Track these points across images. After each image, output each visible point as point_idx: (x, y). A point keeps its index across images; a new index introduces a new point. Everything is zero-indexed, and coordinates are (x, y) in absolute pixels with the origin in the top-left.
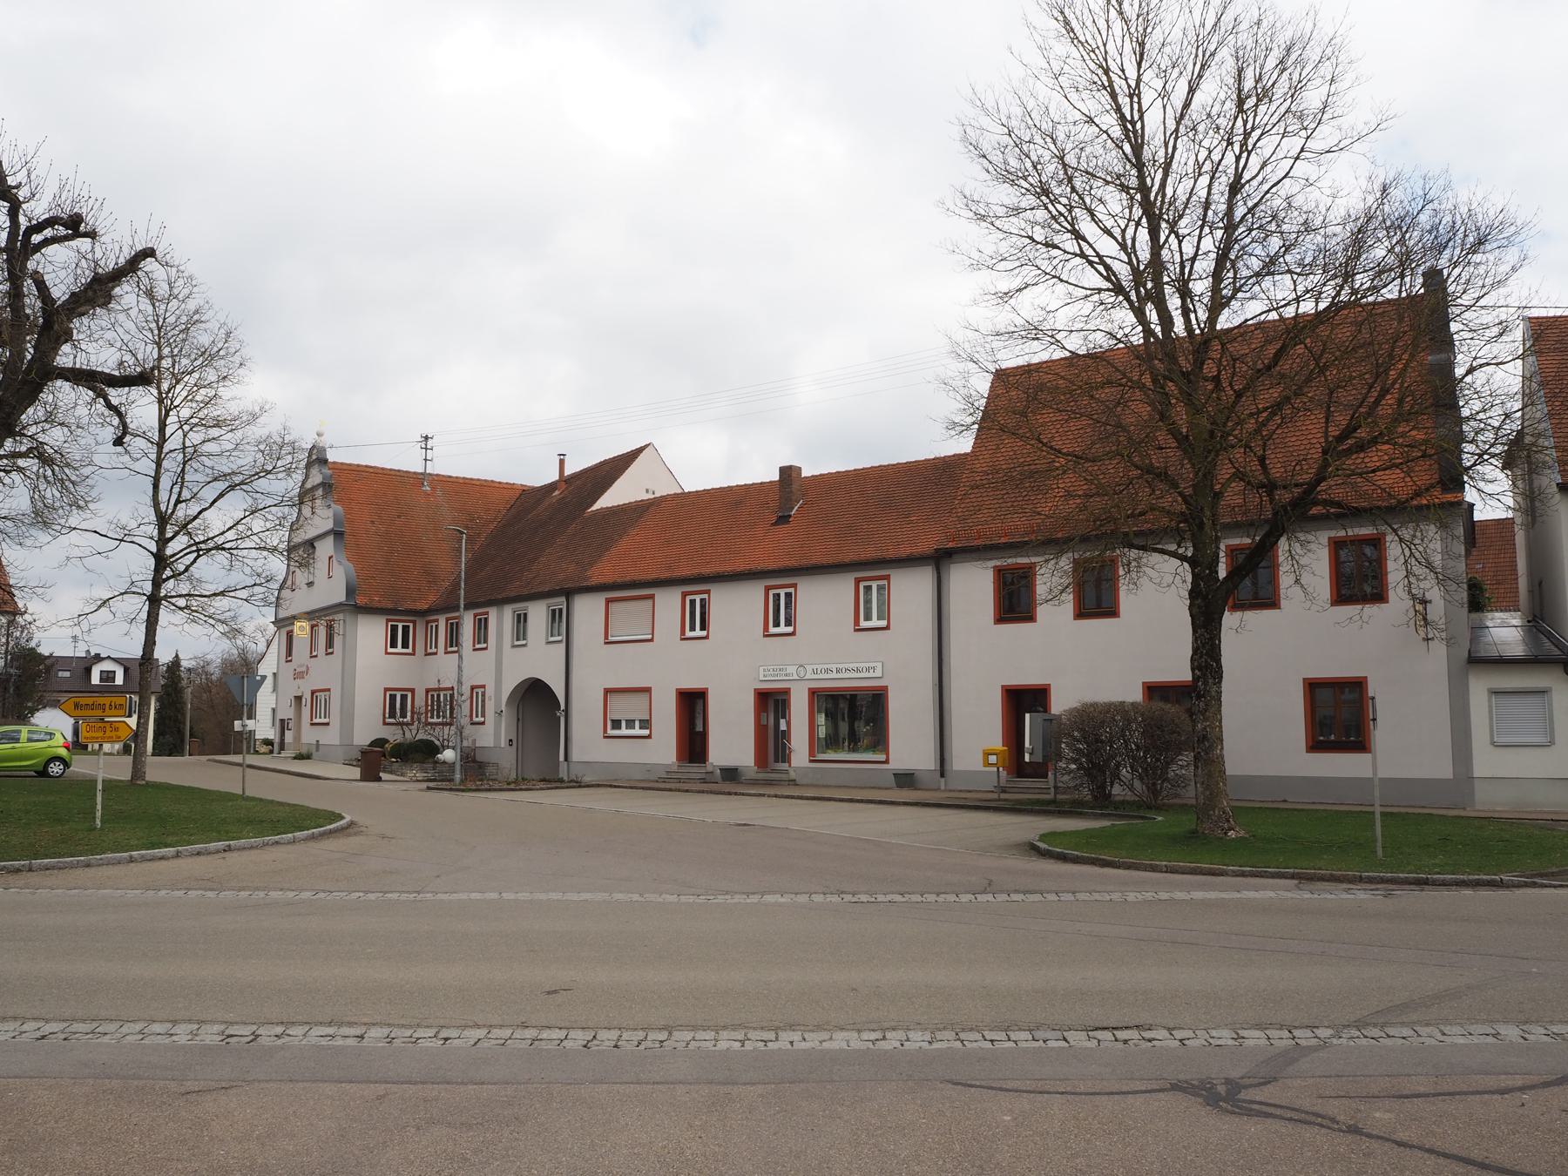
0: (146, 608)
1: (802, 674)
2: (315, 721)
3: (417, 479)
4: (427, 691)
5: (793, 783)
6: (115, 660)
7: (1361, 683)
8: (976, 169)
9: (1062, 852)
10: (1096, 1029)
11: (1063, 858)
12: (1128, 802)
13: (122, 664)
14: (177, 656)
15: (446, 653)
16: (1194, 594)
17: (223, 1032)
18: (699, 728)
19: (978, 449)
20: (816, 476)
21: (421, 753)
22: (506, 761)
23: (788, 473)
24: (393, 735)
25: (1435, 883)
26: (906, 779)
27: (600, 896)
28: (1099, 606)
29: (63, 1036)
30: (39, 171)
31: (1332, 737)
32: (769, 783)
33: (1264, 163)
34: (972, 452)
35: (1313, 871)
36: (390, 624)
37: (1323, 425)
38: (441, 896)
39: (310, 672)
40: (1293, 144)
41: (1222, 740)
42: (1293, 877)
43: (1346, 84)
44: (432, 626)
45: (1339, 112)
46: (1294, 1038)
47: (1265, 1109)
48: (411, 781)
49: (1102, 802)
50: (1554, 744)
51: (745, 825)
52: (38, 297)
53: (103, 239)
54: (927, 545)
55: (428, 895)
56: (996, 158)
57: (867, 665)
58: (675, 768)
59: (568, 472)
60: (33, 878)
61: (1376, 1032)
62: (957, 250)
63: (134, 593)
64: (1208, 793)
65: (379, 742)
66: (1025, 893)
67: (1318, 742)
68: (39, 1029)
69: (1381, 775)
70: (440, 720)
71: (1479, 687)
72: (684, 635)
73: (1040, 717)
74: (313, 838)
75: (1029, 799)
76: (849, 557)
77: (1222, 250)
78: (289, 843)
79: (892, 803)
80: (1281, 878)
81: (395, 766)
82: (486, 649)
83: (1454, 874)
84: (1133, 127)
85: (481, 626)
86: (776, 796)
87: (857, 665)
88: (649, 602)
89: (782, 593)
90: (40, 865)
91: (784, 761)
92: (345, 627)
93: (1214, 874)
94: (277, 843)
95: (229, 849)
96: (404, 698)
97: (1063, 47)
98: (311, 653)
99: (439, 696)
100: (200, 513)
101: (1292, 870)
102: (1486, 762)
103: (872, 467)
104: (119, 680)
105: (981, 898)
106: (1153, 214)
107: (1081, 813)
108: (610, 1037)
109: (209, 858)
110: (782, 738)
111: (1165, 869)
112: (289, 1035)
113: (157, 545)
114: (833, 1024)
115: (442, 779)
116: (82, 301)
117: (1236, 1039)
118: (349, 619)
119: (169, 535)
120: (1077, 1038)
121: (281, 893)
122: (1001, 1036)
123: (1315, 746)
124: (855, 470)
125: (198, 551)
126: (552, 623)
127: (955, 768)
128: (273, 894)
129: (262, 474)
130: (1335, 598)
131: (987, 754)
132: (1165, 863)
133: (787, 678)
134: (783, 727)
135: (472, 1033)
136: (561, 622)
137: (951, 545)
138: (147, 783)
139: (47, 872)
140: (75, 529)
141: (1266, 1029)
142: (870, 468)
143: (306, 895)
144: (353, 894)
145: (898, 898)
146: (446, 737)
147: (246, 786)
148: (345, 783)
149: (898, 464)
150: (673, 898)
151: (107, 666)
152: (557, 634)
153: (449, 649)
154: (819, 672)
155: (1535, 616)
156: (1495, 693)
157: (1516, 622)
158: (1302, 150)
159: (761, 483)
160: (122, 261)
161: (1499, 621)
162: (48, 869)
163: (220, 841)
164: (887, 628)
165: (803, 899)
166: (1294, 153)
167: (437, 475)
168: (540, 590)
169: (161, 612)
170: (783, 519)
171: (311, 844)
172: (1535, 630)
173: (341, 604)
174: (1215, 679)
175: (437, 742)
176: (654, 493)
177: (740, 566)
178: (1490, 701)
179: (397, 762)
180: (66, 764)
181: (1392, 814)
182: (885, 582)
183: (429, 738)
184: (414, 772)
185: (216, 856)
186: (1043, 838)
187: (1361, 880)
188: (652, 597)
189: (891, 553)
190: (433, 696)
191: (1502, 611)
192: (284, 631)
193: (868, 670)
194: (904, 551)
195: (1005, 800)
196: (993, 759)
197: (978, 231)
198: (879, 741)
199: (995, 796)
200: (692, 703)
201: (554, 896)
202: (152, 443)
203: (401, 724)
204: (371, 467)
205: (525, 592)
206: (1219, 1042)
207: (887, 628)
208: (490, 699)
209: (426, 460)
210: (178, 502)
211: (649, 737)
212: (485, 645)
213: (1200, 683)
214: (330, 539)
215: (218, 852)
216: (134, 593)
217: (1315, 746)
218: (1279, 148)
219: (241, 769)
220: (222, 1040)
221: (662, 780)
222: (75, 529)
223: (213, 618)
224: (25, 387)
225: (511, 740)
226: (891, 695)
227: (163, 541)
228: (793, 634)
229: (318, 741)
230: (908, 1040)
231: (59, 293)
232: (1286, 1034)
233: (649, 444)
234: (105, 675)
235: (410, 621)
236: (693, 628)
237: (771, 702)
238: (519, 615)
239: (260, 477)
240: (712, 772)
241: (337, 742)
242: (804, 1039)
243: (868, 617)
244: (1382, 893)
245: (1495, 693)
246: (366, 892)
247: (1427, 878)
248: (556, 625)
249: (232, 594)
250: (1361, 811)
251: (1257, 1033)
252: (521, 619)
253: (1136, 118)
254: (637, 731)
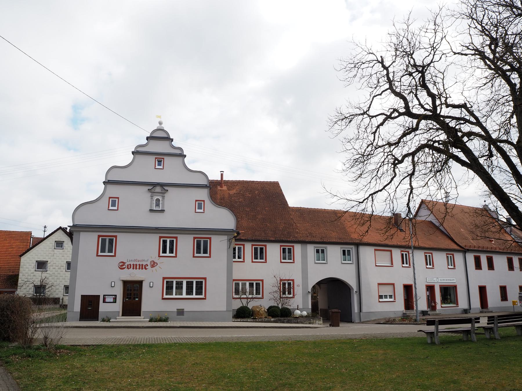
36: (282, 247)
67: (502, 300)
77: (516, 178)
87: (450, 279)
193: (453, 280)
200: (408, 289)
226: (163, 277)
237: (430, 289)
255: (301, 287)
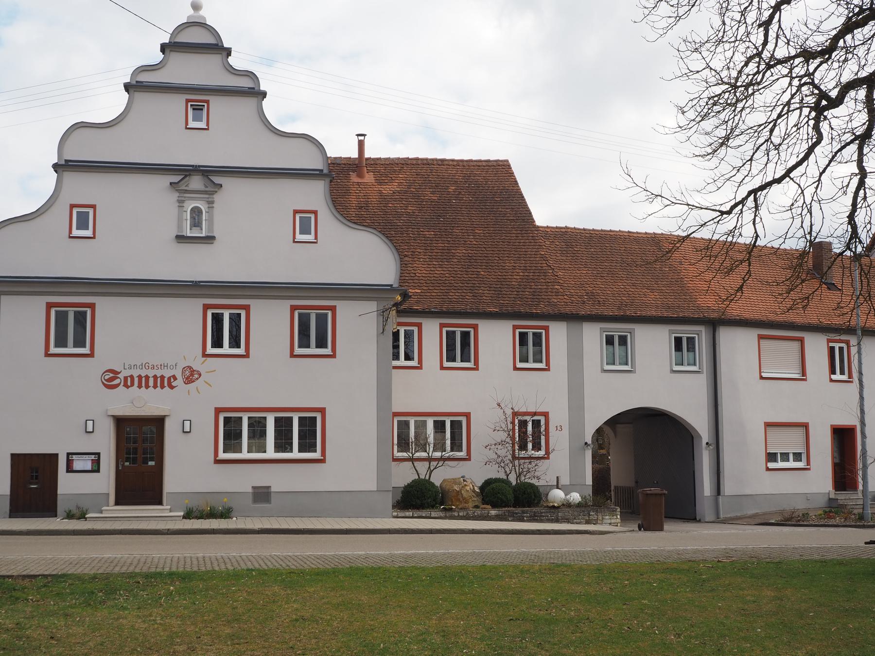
208: (560, 428)
241: (373, 487)
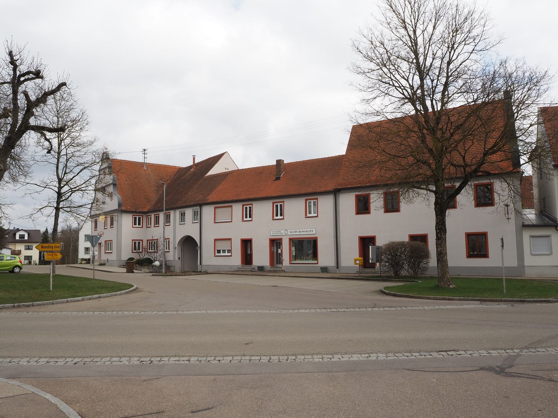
0: (54, 211)
1: (286, 233)
2: (106, 252)
3: (142, 165)
4: (148, 241)
5: (284, 271)
6: (25, 231)
7: (485, 234)
8: (360, 57)
9: (395, 294)
10: (440, 352)
11: (395, 295)
12: (407, 276)
13: (27, 232)
14: (47, 229)
15: (154, 227)
16: (436, 204)
17: (139, 360)
18: (249, 252)
19: (348, 153)
20: (289, 163)
21: (146, 263)
22: (178, 266)
23: (279, 162)
24: (136, 256)
25: (527, 302)
26: (324, 269)
27: (242, 311)
28: (393, 208)
29: (83, 363)
30: (25, 54)
31: (475, 253)
32: (275, 271)
33: (459, 54)
34: (345, 155)
35: (485, 298)
36: (134, 216)
37: (483, 147)
38: (185, 312)
39: (104, 234)
40: (470, 48)
41: (447, 254)
42: (478, 300)
43: (489, 27)
44: (149, 217)
45: (487, 37)
46: (507, 353)
47: (519, 375)
48: (144, 273)
49: (397, 277)
50: (552, 254)
51: (275, 286)
52: (26, 100)
53: (45, 79)
54: (331, 187)
55: (181, 312)
56: (364, 52)
57: (310, 230)
58: (241, 267)
59: (196, 162)
60: (36, 308)
61: (533, 350)
62: (352, 84)
63: (50, 206)
64: (442, 272)
65: (131, 259)
66: (389, 307)
68: (72, 360)
69: (505, 265)
70: (153, 251)
71: (526, 235)
72: (274, 218)
73: (374, 247)
74: (126, 293)
75: (373, 276)
76: (303, 192)
78: (119, 295)
79: (322, 278)
80: (474, 301)
81: (138, 267)
82: (170, 225)
83: (533, 298)
84: (414, 41)
85: (168, 218)
86: (280, 276)
87: (306, 230)
88: (231, 208)
89: (279, 204)
90: (36, 304)
91: (280, 264)
92: (118, 218)
93: (450, 300)
94: (116, 295)
95: (100, 297)
96: (139, 243)
97: (391, 14)
98: (104, 227)
99: (152, 242)
100: (73, 177)
101: (477, 298)
102: (529, 261)
103: (309, 160)
104: (26, 238)
105: (375, 309)
106: (422, 72)
107: (391, 280)
108: (276, 358)
109: (94, 300)
110: (279, 256)
111: (433, 299)
112: (163, 361)
113: (58, 189)
114: (350, 352)
115: (157, 271)
116: (40, 101)
117: (488, 354)
118: (119, 215)
119: (62, 185)
120: (435, 354)
121: (128, 312)
122: (409, 354)
123: (469, 256)
124: (303, 161)
125: (72, 191)
126: (194, 216)
127: (342, 265)
128: (125, 313)
129: (95, 164)
130: (476, 204)
131: (356, 260)
132: (433, 296)
133: (281, 234)
134: (279, 251)
135: (227, 358)
136: (198, 217)
137: (340, 187)
138: (56, 274)
139: (39, 306)
140: (28, 183)
141: (496, 350)
142: (308, 160)
143: (137, 313)
144: (154, 312)
145: (346, 310)
146: (155, 257)
147: (95, 275)
148: (121, 274)
149: (318, 159)
150: (268, 311)
151: (22, 233)
152: (183, 221)
153: (156, 226)
154: (293, 232)
155: (541, 210)
156: (532, 237)
157: (534, 212)
158: (473, 50)
159: (269, 166)
160: (54, 88)
161: (528, 212)
162: (39, 305)
163: (97, 294)
164: (317, 216)
165: (313, 311)
166: (470, 51)
167: (148, 163)
168: (190, 204)
169: (60, 213)
170: (278, 178)
171: (127, 295)
172: (541, 215)
173: (116, 210)
174: (444, 233)
175: (152, 259)
176: (228, 169)
177: (263, 195)
178: (530, 239)
179: (138, 266)
180: (21, 268)
181: (498, 279)
182: (316, 200)
183: (149, 257)
184: (145, 269)
185: (97, 300)
186: (385, 288)
187: (501, 301)
188: (231, 206)
189: (318, 190)
190: (149, 242)
191: (528, 209)
192: (93, 220)
193: (310, 231)
194: (323, 189)
195: (362, 276)
196: (358, 262)
197: (360, 77)
198: (315, 256)
199: (358, 275)
200: (246, 244)
201: (227, 311)
202: (55, 152)
203: (139, 252)
204: (125, 160)
205: (184, 205)
206: (483, 355)
207: (317, 216)
208: (171, 243)
209: (145, 158)
210: (65, 173)
211: (231, 256)
212: (169, 224)
213: (439, 234)
214: (112, 186)
215: (96, 298)
216: (50, 206)
217: (469, 256)
218: (463, 49)
219: (93, 271)
220: (140, 363)
221: (236, 271)
222: (28, 183)
223: (79, 215)
224: (20, 132)
225: (179, 258)
227: (60, 188)
228: (283, 219)
229: (108, 259)
230: (378, 357)
231: (33, 98)
232: (504, 351)
233: (226, 152)
234: (21, 236)
235: (141, 216)
236: (246, 217)
237: (275, 243)
238: (182, 213)
239: (95, 165)
240: (254, 268)
242: (343, 357)
243: (310, 213)
244: (511, 305)
245: (532, 237)
246: (158, 311)
247: (524, 300)
248: (196, 217)
249: (85, 206)
250: (487, 278)
251: (494, 352)
252: (183, 215)
253: (415, 39)
254: (226, 254)
255: (172, 244)
